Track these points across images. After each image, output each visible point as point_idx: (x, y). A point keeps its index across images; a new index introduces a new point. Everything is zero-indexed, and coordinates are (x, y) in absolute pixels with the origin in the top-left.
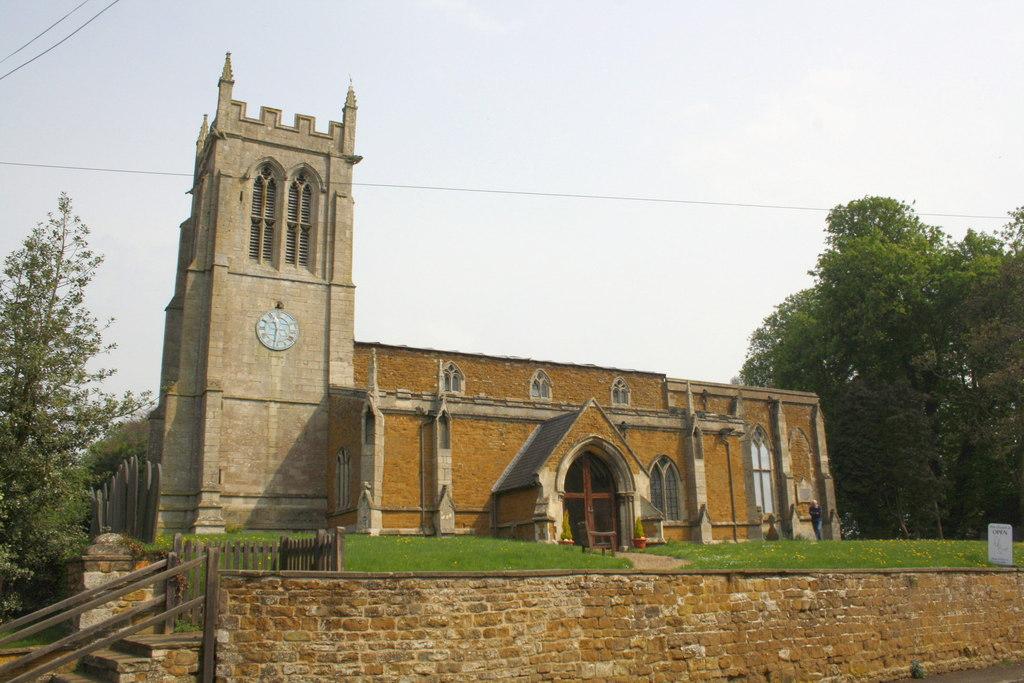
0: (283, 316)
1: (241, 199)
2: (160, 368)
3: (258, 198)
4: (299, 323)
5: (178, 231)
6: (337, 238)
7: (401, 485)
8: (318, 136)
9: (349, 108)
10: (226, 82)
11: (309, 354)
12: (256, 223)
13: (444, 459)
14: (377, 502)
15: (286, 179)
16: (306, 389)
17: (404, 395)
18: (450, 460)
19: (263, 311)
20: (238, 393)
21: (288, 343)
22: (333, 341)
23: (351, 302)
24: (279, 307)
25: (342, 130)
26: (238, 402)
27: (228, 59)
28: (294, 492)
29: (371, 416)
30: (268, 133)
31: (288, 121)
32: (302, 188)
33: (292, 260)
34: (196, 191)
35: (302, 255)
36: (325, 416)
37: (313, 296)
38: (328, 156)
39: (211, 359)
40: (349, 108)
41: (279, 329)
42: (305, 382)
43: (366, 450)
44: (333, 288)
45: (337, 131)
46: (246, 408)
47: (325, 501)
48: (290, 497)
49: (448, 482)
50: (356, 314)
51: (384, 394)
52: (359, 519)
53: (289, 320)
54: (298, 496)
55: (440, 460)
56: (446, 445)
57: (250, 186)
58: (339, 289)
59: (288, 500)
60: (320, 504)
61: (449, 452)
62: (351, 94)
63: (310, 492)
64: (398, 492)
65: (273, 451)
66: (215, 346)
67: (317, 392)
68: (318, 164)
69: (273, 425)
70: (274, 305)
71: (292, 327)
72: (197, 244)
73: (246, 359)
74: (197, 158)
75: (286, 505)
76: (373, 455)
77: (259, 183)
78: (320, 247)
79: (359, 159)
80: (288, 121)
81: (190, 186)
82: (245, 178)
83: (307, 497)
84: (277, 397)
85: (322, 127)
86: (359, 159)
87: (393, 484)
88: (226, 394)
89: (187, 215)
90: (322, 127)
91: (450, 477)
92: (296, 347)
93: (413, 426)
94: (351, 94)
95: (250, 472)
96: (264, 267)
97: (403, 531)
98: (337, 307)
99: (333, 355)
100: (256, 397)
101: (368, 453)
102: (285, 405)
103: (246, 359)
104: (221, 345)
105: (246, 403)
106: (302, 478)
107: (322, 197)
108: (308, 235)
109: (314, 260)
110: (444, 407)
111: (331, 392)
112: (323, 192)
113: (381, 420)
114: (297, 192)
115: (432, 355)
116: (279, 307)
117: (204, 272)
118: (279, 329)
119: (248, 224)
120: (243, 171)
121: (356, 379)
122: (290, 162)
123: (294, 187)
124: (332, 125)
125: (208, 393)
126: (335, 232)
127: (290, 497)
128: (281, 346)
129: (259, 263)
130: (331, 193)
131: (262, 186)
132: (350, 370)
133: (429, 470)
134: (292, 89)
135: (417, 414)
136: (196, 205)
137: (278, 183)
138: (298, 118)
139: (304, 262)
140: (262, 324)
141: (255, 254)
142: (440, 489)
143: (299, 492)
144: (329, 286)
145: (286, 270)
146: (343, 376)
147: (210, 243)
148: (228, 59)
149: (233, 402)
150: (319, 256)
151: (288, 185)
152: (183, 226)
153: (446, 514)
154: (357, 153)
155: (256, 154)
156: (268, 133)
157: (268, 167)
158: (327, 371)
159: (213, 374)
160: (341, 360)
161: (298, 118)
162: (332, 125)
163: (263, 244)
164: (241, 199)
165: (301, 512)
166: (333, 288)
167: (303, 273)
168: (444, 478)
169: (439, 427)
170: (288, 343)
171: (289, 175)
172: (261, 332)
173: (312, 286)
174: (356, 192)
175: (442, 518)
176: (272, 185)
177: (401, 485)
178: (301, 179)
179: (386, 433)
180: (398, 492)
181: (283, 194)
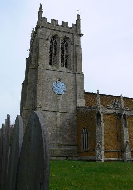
0: (61, 83)
1: (46, 46)
2: (20, 103)
3: (51, 47)
4: (66, 85)
5: (25, 61)
6: (77, 59)
7: (110, 142)
8: (69, 28)
9: (78, 20)
10: (40, 12)
11: (70, 96)
12: (51, 54)
13: (126, 131)
14: (103, 148)
15: (60, 40)
16: (69, 108)
17: (110, 108)
18: (128, 132)
19: (55, 83)
20: (47, 109)
21: (63, 92)
22: (78, 92)
23: (83, 79)
24: (59, 80)
25: (77, 26)
26: (47, 112)
27: (41, 5)
28: (66, 143)
29: (99, 115)
30: (54, 27)
31: (60, 23)
32: (65, 44)
33: (62, 66)
34: (31, 50)
35: (65, 64)
36: (76, 117)
37: (71, 77)
38: (73, 34)
39: (38, 96)
40: (78, 20)
41: (59, 88)
42: (68, 105)
43: (98, 128)
44: (77, 74)
45: (75, 27)
46: (49, 114)
47: (77, 147)
48: (65, 145)
49: (128, 140)
50: (84, 85)
51: (103, 107)
52: (96, 155)
53: (63, 85)
54: (67, 145)
55: (124, 132)
56: (126, 126)
57: (49, 42)
58: (79, 75)
59: (64, 146)
60: (75, 148)
61: (127, 129)
62: (78, 16)
63: (72, 143)
64: (109, 144)
65: (59, 129)
66: (39, 92)
67: (72, 108)
68: (70, 36)
69: (59, 120)
70: (58, 79)
71: (64, 87)
72: (32, 65)
73: (49, 97)
74: (31, 40)
75: (64, 148)
76: (101, 130)
77: (51, 42)
78: (72, 62)
79: (82, 35)
80: (60, 23)
81: (29, 48)
82: (47, 40)
83: (71, 145)
84: (60, 110)
85: (70, 25)
86: (82, 35)
87: (108, 141)
88: (43, 109)
89: (28, 56)
90: (70, 25)
91: (128, 138)
92: (65, 94)
93: (113, 119)
94: (78, 16)
95: (51, 136)
96: (54, 68)
97: (112, 159)
98: (78, 80)
99: (78, 96)
100: (53, 110)
101: (99, 129)
102: (62, 113)
103: (49, 97)
104: (41, 92)
105: (50, 112)
106: (69, 138)
107: (72, 46)
108: (67, 58)
109: (70, 66)
110: (124, 112)
111: (78, 109)
112: (72, 45)
113: (102, 116)
114: (63, 45)
115: (109, 97)
116: (59, 80)
117: (35, 69)
118: (59, 88)
119: (48, 54)
120: (47, 37)
121: (85, 105)
122: (61, 35)
123: (62, 43)
124: (73, 25)
125: (37, 108)
126: (77, 57)
127: (65, 145)
128: (61, 93)
129: (52, 67)
130: (74, 45)
131: (52, 43)
132: (84, 102)
133: (120, 135)
134: (61, 13)
135: (115, 115)
136: (31, 53)
137: (57, 42)
138: (63, 22)
139: (66, 67)
140: (54, 86)
141: (51, 64)
142: (125, 142)
143: (68, 143)
144: (75, 74)
145: (61, 68)
146: (81, 103)
147: (36, 60)
148: (41, 5)
149: (45, 112)
150: (72, 64)
151: (61, 42)
152: (27, 59)
153: (128, 152)
154: (82, 33)
155: (49, 33)
156: (54, 27)
157: (54, 37)
158: (76, 102)
159: (38, 102)
160: (81, 98)
161: (63, 22)
162: (73, 25)
163: (53, 61)
164: (46, 46)
165: (68, 151)
166: (77, 74)
167: (66, 69)
168: (126, 139)
169: (123, 120)
170: (63, 92)
171: (61, 39)
172: (54, 88)
173: (70, 74)
174: (82, 45)
175: (127, 154)
176: (56, 43)
177: (110, 142)
178: (65, 41)
179: (104, 122)
180: (109, 144)
181: (59, 45)
